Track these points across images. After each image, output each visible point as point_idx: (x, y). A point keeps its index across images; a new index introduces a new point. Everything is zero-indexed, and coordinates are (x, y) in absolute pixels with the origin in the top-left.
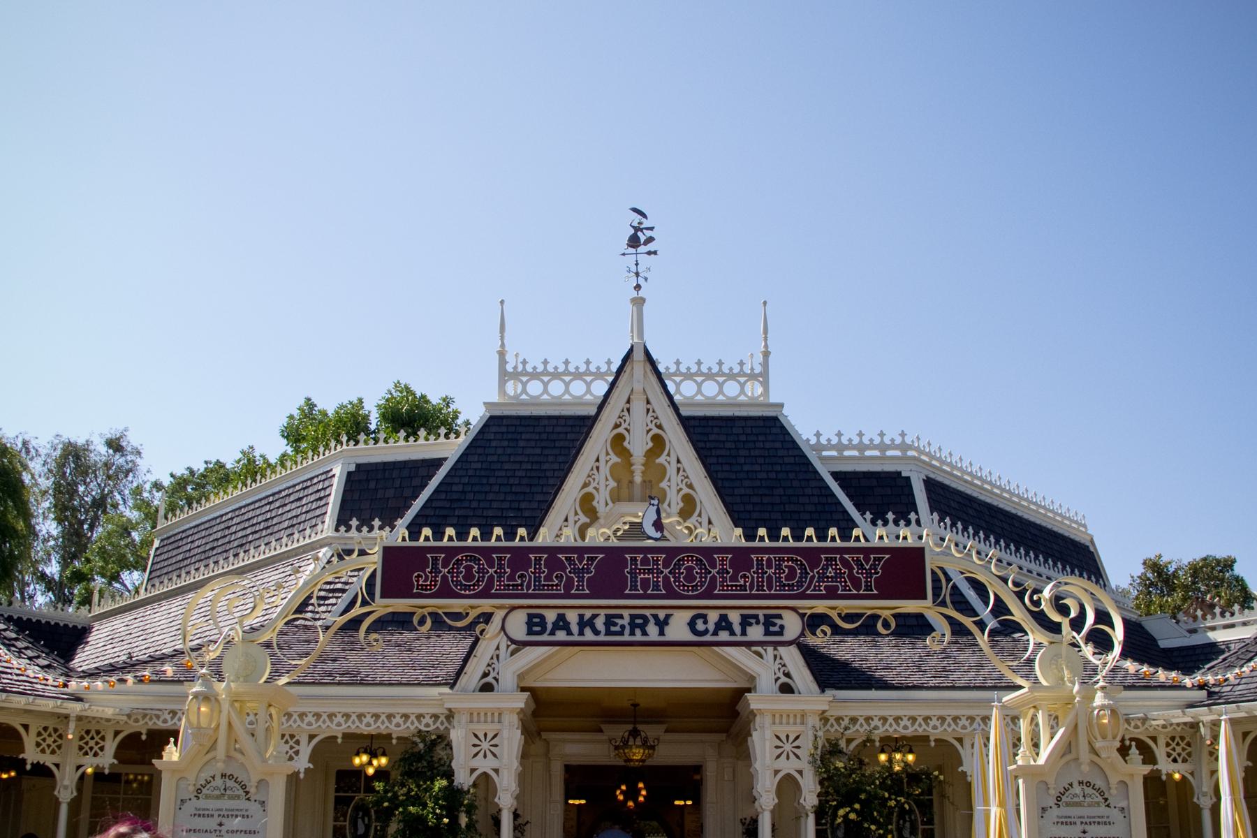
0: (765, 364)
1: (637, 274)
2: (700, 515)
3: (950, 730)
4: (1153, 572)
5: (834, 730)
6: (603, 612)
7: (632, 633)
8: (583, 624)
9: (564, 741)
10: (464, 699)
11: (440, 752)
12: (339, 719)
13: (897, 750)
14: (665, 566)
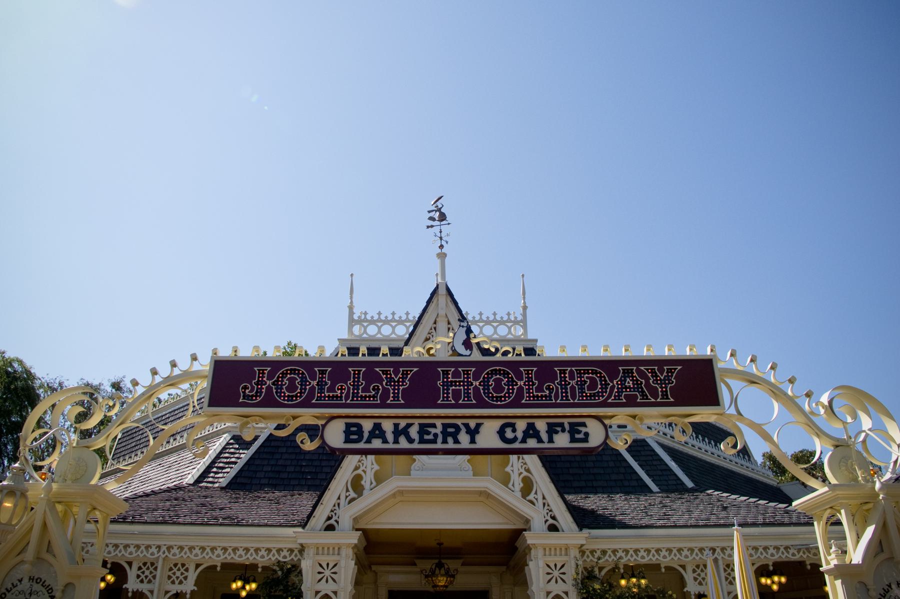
0: (524, 315)
1: (441, 238)
3: (676, 559)
4: (770, 461)
5: (591, 560)
6: (417, 422)
7: (445, 441)
8: (398, 432)
9: (388, 572)
10: (313, 536)
11: (293, 578)
12: (219, 551)
13: (633, 576)
14: (475, 379)
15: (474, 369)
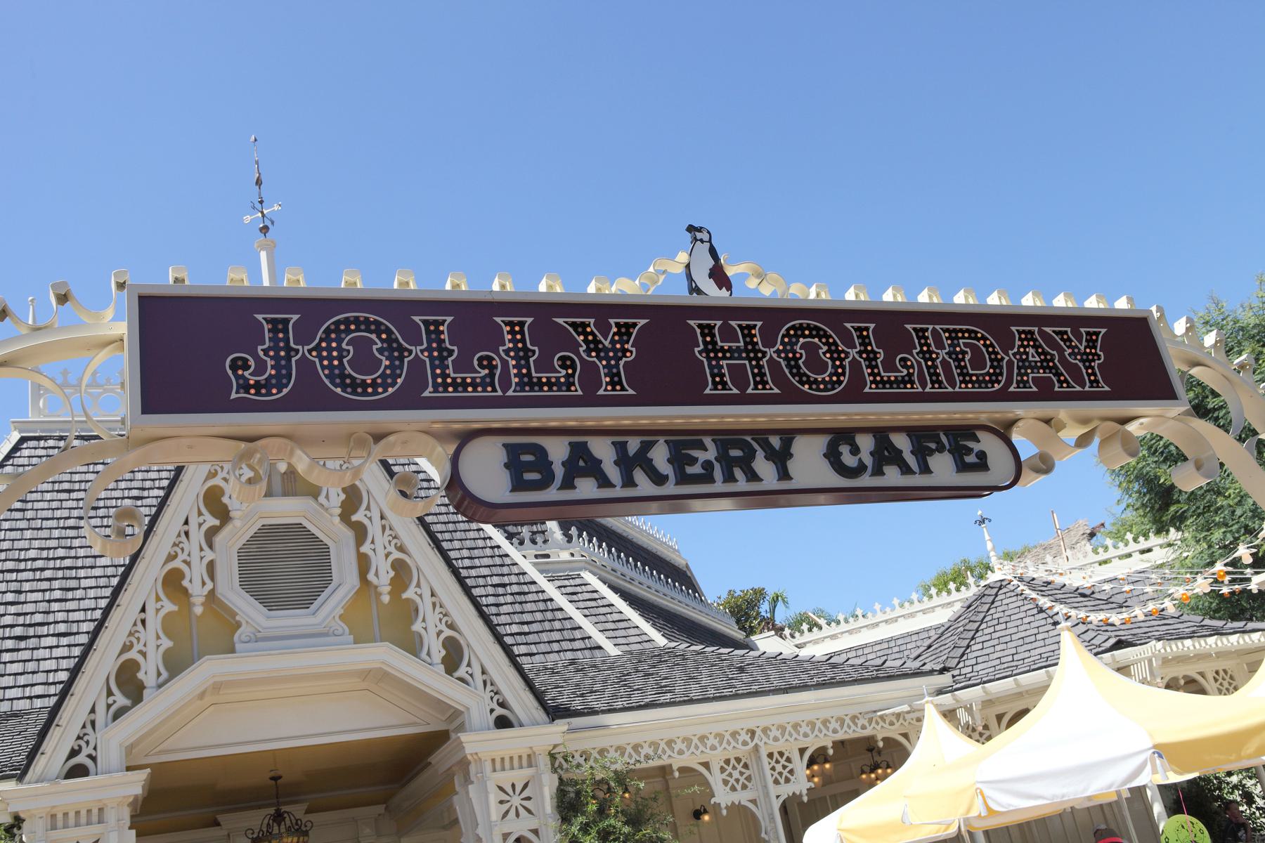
2: (368, 508)
7: (730, 478)
15: (449, 319)
